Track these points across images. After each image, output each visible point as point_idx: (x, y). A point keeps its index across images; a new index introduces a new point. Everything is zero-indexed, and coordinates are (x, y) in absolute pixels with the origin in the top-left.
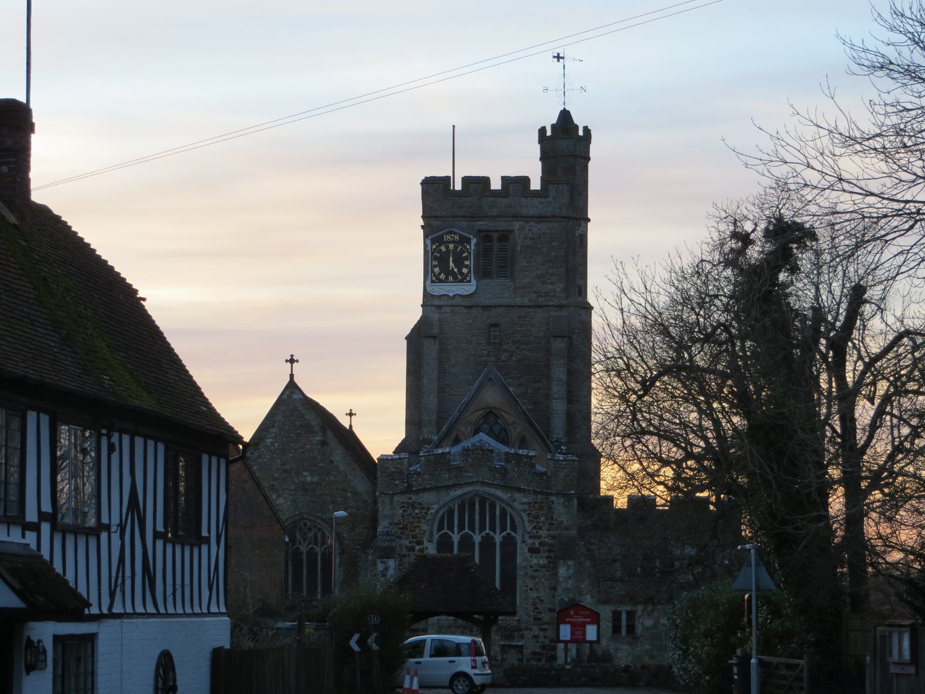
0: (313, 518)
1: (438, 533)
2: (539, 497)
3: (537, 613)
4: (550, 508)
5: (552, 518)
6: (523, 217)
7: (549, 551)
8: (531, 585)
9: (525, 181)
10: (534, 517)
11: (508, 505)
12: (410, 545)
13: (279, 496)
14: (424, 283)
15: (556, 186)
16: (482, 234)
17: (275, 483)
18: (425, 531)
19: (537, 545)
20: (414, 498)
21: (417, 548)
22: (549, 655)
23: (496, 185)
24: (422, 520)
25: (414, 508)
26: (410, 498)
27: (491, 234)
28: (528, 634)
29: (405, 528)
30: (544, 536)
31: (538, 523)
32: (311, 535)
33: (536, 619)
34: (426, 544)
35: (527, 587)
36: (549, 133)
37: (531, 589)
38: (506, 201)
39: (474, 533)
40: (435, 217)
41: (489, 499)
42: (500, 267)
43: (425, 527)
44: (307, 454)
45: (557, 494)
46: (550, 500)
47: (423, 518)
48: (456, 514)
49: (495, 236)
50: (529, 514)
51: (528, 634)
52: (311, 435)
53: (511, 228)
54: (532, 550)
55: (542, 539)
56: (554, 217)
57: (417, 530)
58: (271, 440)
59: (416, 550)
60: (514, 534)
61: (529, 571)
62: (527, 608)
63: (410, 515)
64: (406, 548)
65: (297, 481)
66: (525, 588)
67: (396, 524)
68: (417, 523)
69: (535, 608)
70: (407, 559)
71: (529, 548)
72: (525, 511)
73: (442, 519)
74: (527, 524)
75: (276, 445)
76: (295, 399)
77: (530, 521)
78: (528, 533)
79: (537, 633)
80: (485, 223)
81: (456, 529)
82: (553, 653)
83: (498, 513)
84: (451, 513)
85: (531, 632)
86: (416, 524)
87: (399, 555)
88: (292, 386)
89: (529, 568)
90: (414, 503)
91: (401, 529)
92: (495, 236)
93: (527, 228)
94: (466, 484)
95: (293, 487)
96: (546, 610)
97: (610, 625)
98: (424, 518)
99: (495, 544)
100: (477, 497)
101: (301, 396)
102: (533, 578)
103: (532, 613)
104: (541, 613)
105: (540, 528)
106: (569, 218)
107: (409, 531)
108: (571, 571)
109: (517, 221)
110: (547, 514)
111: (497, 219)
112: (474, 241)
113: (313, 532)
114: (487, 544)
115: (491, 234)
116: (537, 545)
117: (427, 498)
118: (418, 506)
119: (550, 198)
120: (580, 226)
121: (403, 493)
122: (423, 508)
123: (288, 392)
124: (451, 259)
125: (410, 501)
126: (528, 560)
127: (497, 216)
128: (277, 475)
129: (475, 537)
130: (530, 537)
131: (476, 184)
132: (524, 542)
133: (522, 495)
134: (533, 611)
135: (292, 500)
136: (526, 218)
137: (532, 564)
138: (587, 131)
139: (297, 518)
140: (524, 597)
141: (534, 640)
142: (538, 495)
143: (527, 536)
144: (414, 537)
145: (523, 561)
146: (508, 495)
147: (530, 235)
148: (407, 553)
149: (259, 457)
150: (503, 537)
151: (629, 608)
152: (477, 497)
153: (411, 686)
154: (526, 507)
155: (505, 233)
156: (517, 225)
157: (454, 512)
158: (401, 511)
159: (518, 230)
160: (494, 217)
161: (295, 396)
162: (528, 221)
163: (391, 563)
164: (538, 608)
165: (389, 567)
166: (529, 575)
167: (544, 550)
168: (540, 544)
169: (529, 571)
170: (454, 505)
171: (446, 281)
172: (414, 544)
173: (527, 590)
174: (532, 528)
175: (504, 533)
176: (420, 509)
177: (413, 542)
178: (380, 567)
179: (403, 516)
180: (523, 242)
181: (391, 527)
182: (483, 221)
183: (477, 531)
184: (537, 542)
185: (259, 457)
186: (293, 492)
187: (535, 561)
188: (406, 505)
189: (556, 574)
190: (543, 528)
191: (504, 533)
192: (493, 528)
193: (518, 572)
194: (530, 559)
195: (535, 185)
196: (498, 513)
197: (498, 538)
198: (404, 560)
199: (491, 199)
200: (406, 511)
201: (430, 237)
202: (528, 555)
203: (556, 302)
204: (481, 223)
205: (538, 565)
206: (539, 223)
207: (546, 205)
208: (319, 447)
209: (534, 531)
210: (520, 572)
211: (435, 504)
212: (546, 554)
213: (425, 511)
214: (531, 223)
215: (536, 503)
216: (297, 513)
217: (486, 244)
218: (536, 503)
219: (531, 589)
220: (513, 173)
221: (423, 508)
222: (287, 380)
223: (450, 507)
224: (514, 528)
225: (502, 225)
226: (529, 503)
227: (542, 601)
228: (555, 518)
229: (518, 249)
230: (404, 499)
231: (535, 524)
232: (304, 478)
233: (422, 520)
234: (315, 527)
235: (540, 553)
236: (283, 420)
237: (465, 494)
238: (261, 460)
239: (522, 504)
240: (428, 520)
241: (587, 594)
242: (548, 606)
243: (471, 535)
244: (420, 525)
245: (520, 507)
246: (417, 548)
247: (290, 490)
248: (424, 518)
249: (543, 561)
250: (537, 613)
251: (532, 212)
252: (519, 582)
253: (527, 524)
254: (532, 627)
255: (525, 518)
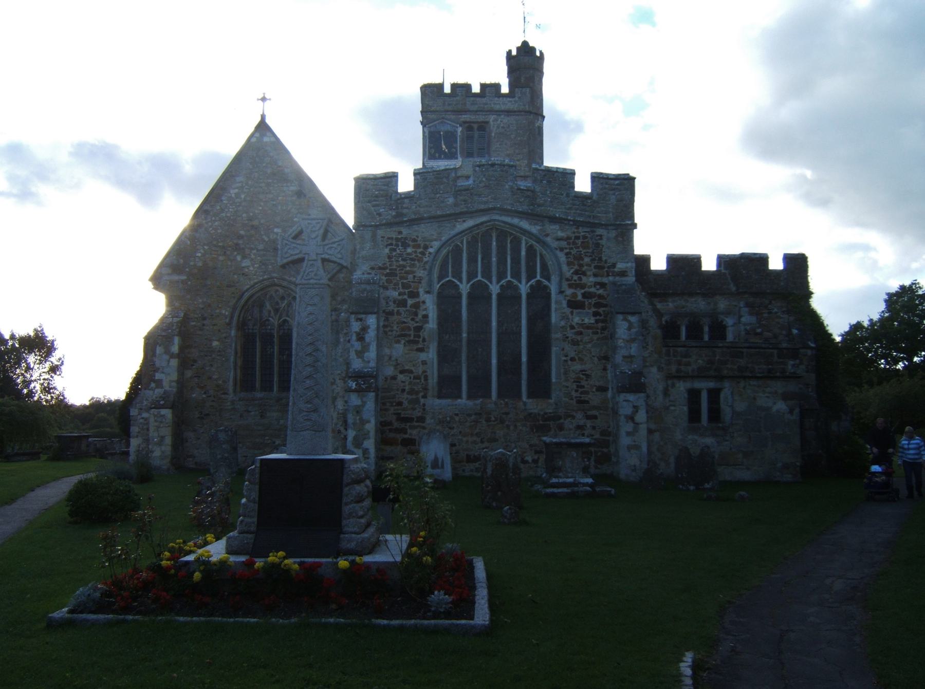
0: (285, 284)
1: (438, 283)
2: (581, 229)
3: (582, 393)
4: (597, 245)
5: (600, 259)
6: (497, 111)
7: (598, 305)
8: (572, 354)
9: (497, 86)
10: (575, 258)
11: (539, 241)
12: (400, 298)
13: (244, 257)
14: (423, 159)
15: (521, 89)
16: (467, 125)
17: (241, 242)
18: (421, 279)
19: (580, 298)
20: (405, 231)
21: (410, 302)
22: (599, 454)
23: (476, 89)
24: (416, 262)
25: (405, 245)
26: (400, 233)
27: (472, 124)
28: (568, 424)
29: (392, 274)
30: (589, 284)
31: (581, 266)
32: (284, 304)
33: (580, 402)
34: (423, 296)
35: (566, 356)
36: (514, 53)
37: (572, 359)
38: (484, 100)
39: (491, 282)
40: (431, 112)
41: (511, 234)
42: (479, 149)
43: (421, 273)
44: (280, 207)
45: (605, 226)
46: (598, 233)
47: (419, 261)
48: (465, 255)
49: (475, 126)
50: (567, 254)
51: (568, 424)
52: (285, 185)
53: (487, 120)
54: (574, 305)
55: (587, 289)
56: (519, 111)
57: (410, 277)
58: (237, 190)
59: (408, 305)
60: (546, 282)
61: (570, 334)
62: (567, 387)
63: (400, 255)
64: (394, 302)
65: (266, 239)
66: (564, 358)
67: (380, 268)
68: (410, 266)
69: (578, 386)
70: (395, 317)
71: (569, 301)
72: (562, 250)
73: (444, 266)
74: (565, 268)
75: (243, 196)
76: (266, 142)
77: (569, 264)
78: (567, 280)
79: (581, 423)
80: (468, 116)
81: (464, 276)
82: (605, 450)
83: (523, 253)
84: (457, 251)
85: (573, 421)
86: (408, 268)
87: (384, 311)
88: (262, 127)
89: (568, 329)
90: (406, 238)
91: (386, 275)
92: (475, 126)
93: (500, 120)
94: (477, 211)
95: (261, 247)
96: (594, 390)
97: (685, 408)
98: (420, 260)
99: (520, 297)
100: (494, 230)
101: (273, 139)
102: (575, 343)
103: (574, 394)
104: (587, 393)
105: (584, 274)
106: (530, 113)
107: (398, 278)
108: (634, 330)
109: (493, 115)
110: (593, 253)
111: (478, 113)
112: (460, 129)
113: (286, 302)
114: (509, 297)
115: (472, 124)
116: (580, 298)
117: (424, 231)
118: (410, 243)
119: (516, 98)
120: (538, 120)
121: (389, 225)
122: (418, 246)
123: (257, 135)
124: (443, 142)
125: (400, 237)
126: (568, 319)
127: (477, 111)
128: (242, 232)
129: (491, 287)
130: (570, 286)
131: (462, 89)
132: (561, 292)
133: (557, 227)
134: (576, 391)
135: (260, 262)
136: (499, 112)
137: (574, 324)
138: (541, 53)
139: (266, 283)
140: (562, 371)
141: (578, 432)
142: (581, 228)
143: (565, 284)
144: (405, 286)
145: (561, 320)
146: (539, 228)
147: (502, 125)
148: (396, 310)
149: (222, 210)
150: (531, 286)
151: (711, 385)
152: (494, 230)
153: (401, 536)
154: (564, 244)
155: (483, 124)
156: (492, 118)
157: (463, 251)
158: (387, 251)
159: (493, 121)
160: (476, 112)
161: (266, 139)
162: (500, 115)
163: (372, 320)
164: (583, 387)
165: (368, 327)
166: (570, 339)
167: (590, 304)
168: (584, 295)
169: (570, 334)
170: (462, 243)
171: (440, 158)
172: (406, 297)
173: (566, 361)
174: (572, 273)
175: (533, 282)
176: (414, 247)
177: (404, 294)
178: (356, 326)
179: (390, 257)
180: (496, 130)
181: (373, 272)
182: (466, 115)
183: (494, 279)
184: (579, 293)
185: (222, 210)
186: (262, 253)
187: (577, 320)
188: (394, 243)
189: (612, 336)
190: (588, 273)
191: (533, 282)
192: (516, 275)
193: (554, 336)
194: (570, 316)
195: (505, 89)
196: (523, 253)
197: (524, 289)
198: (392, 319)
199: (472, 99)
200: (395, 250)
201: (427, 126)
202: (568, 311)
203: (522, 174)
204: (465, 116)
205: (582, 325)
206: (508, 116)
207: (513, 102)
208: (294, 198)
209: (575, 277)
210: (556, 335)
211: (436, 240)
212: (593, 310)
213: (421, 250)
214: (502, 116)
215: (577, 238)
216: (265, 277)
217: (468, 133)
218: (577, 238)
219: (572, 359)
220: (488, 81)
221: (418, 246)
222: (259, 119)
223: (457, 246)
224: (547, 277)
225: (481, 118)
226: (568, 238)
227: (588, 376)
228: (604, 259)
229: (493, 135)
230: (392, 233)
231: (576, 267)
232: (275, 236)
233: (416, 262)
234: (289, 295)
235: (584, 309)
236: (251, 167)
237: (477, 225)
238: (224, 215)
239: (558, 239)
240: (426, 263)
241: (652, 366)
242: (597, 384)
243: (486, 285)
244: (415, 269)
245: (555, 244)
246: (410, 302)
247: (258, 250)
248: (420, 260)
249: (589, 320)
250: (582, 393)
251: (503, 108)
252: (554, 349)
253: (565, 268)
254: (574, 414)
255: (563, 258)
